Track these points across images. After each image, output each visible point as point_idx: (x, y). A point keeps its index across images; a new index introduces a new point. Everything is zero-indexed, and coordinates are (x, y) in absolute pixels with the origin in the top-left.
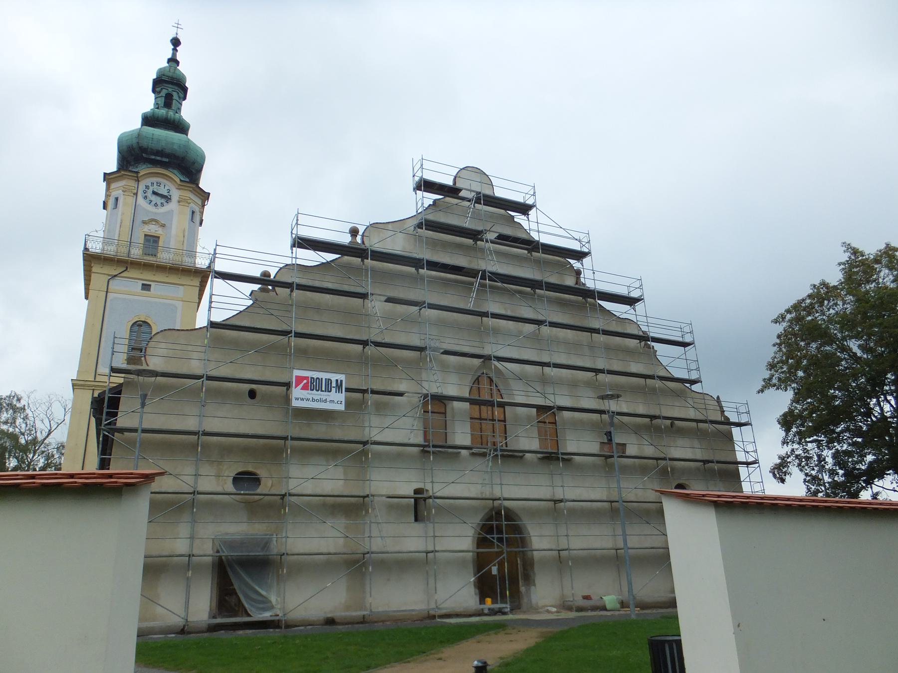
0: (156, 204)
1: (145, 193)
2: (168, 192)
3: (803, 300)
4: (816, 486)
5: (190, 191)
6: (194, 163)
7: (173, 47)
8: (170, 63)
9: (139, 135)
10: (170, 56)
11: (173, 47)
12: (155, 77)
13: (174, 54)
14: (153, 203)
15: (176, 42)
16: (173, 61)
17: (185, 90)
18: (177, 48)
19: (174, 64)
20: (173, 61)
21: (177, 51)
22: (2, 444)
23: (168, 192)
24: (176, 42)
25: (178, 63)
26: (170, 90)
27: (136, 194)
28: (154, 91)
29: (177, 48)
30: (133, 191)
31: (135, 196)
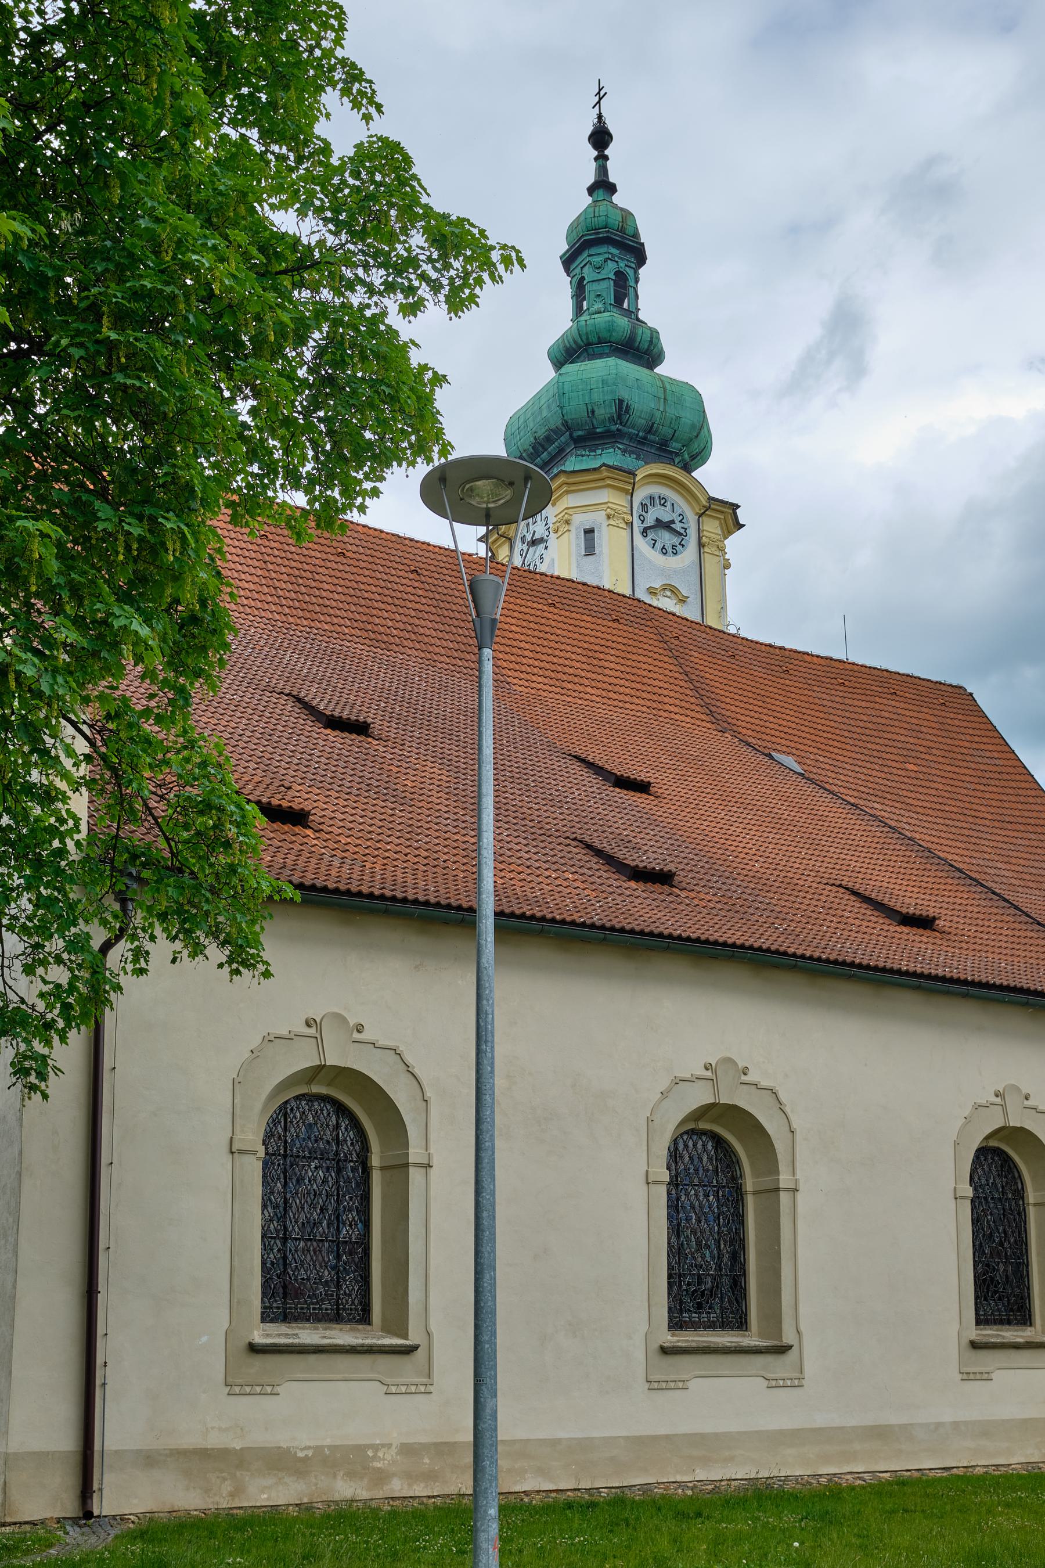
0: (663, 548)
1: (643, 522)
2: (681, 521)
3: (472, 225)
4: (61, 931)
5: (567, 492)
6: (593, 412)
7: (595, 153)
8: (595, 194)
9: (558, 393)
10: (591, 179)
11: (595, 153)
12: (565, 247)
13: (602, 170)
14: (659, 545)
15: (601, 138)
16: (603, 186)
17: (639, 255)
18: (606, 152)
19: (600, 194)
20: (603, 186)
21: (606, 158)
22: (2, 875)
23: (681, 521)
24: (601, 138)
25: (612, 189)
26: (622, 264)
27: (631, 525)
28: (568, 262)
29: (606, 152)
30: (625, 516)
31: (629, 530)
